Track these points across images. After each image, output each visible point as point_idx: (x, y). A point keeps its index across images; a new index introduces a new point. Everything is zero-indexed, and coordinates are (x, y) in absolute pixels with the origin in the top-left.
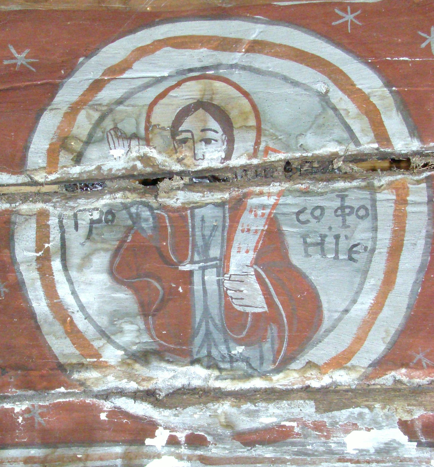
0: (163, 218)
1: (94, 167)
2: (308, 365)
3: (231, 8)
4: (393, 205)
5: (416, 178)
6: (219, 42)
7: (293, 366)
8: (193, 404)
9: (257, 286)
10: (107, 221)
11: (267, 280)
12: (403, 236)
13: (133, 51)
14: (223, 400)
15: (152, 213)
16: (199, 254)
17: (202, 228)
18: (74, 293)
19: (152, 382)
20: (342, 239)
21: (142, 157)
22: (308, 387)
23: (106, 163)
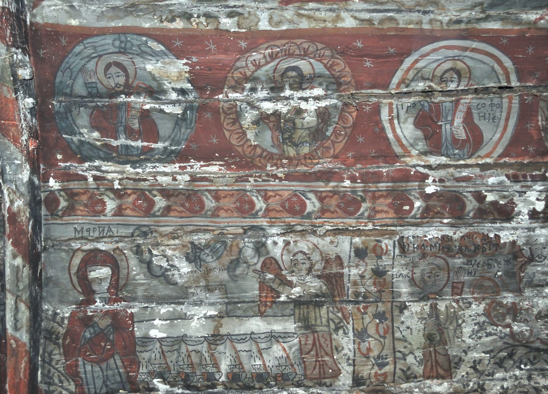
7: (473, 157)
15: (428, 104)
18: (402, 132)
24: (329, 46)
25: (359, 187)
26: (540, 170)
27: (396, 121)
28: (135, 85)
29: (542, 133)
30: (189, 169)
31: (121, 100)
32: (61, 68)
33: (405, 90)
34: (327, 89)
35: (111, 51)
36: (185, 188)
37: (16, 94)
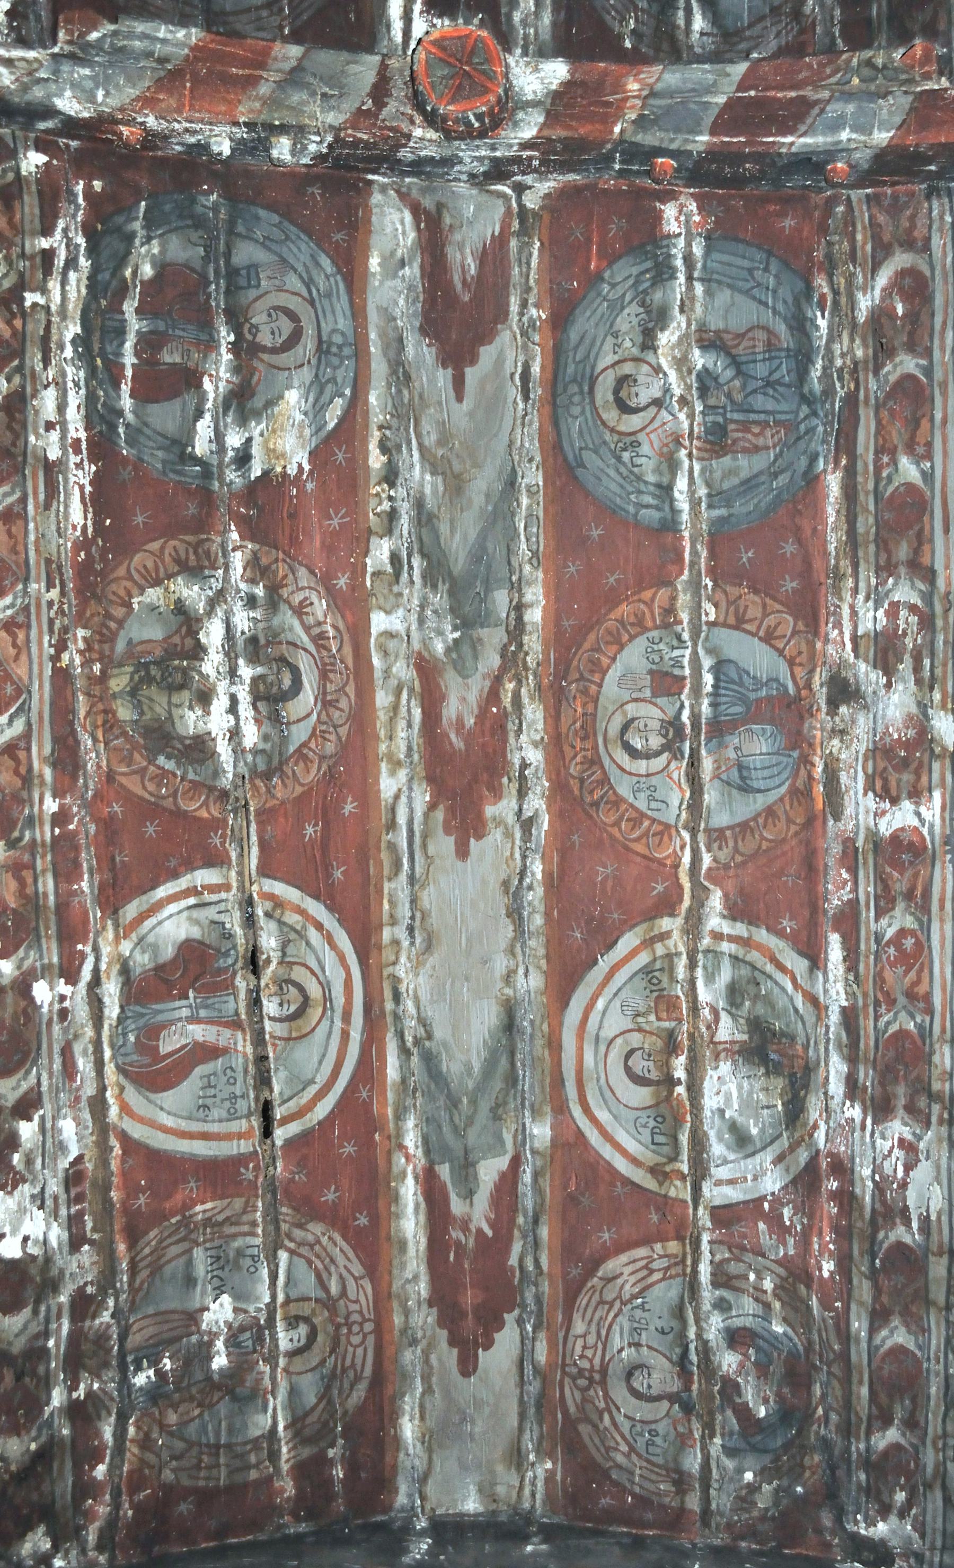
7: (121, 1078)
24: (345, 747)
25: (42, 833)
26: (94, 1229)
27: (192, 901)
28: (256, 363)
29: (178, 1218)
30: (73, 459)
31: (223, 333)
32: (286, 224)
33: (260, 912)
34: (255, 752)
35: (323, 325)
36: (30, 448)
37: (246, 124)
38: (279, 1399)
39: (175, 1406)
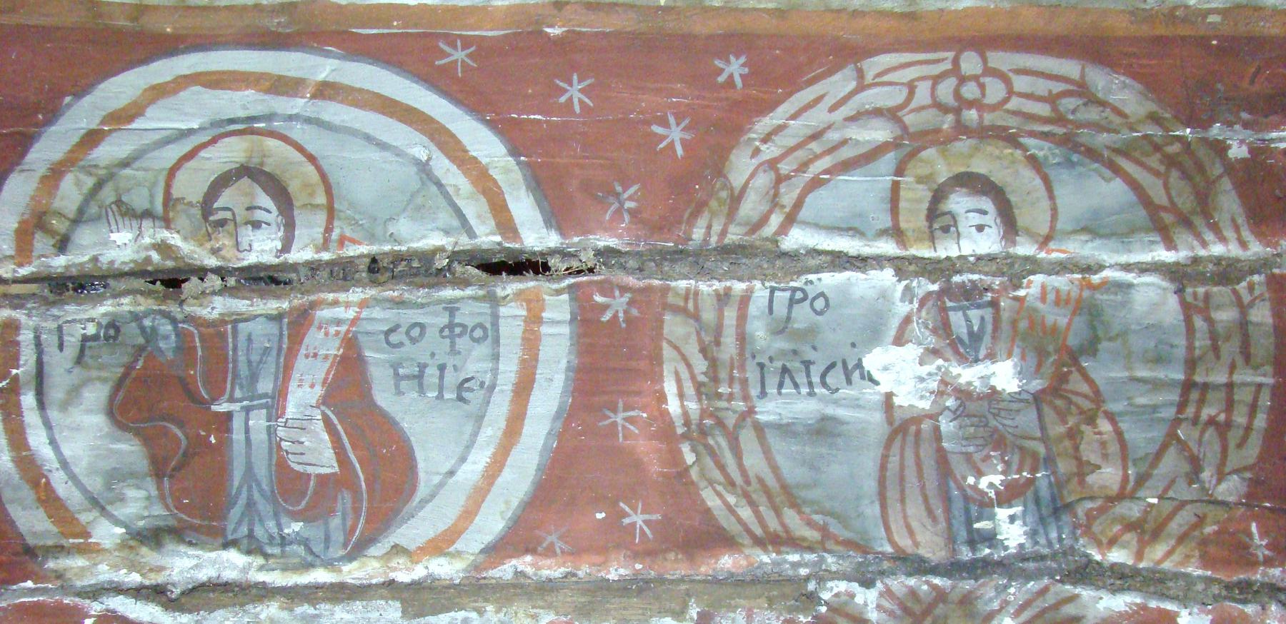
0: (192, 335)
1: (86, 258)
2: (394, 551)
3: (288, 35)
4: (522, 323)
5: (555, 286)
6: (272, 82)
7: (374, 551)
8: (225, 606)
9: (326, 437)
10: (107, 338)
11: (339, 427)
12: (535, 367)
13: (146, 90)
14: (269, 601)
15: (176, 328)
16: (242, 387)
17: (248, 350)
18: (53, 442)
19: (163, 573)
20: (449, 369)
21: (159, 245)
22: (393, 581)
23: (105, 251)
38: (1107, 257)
39: (1083, 469)
